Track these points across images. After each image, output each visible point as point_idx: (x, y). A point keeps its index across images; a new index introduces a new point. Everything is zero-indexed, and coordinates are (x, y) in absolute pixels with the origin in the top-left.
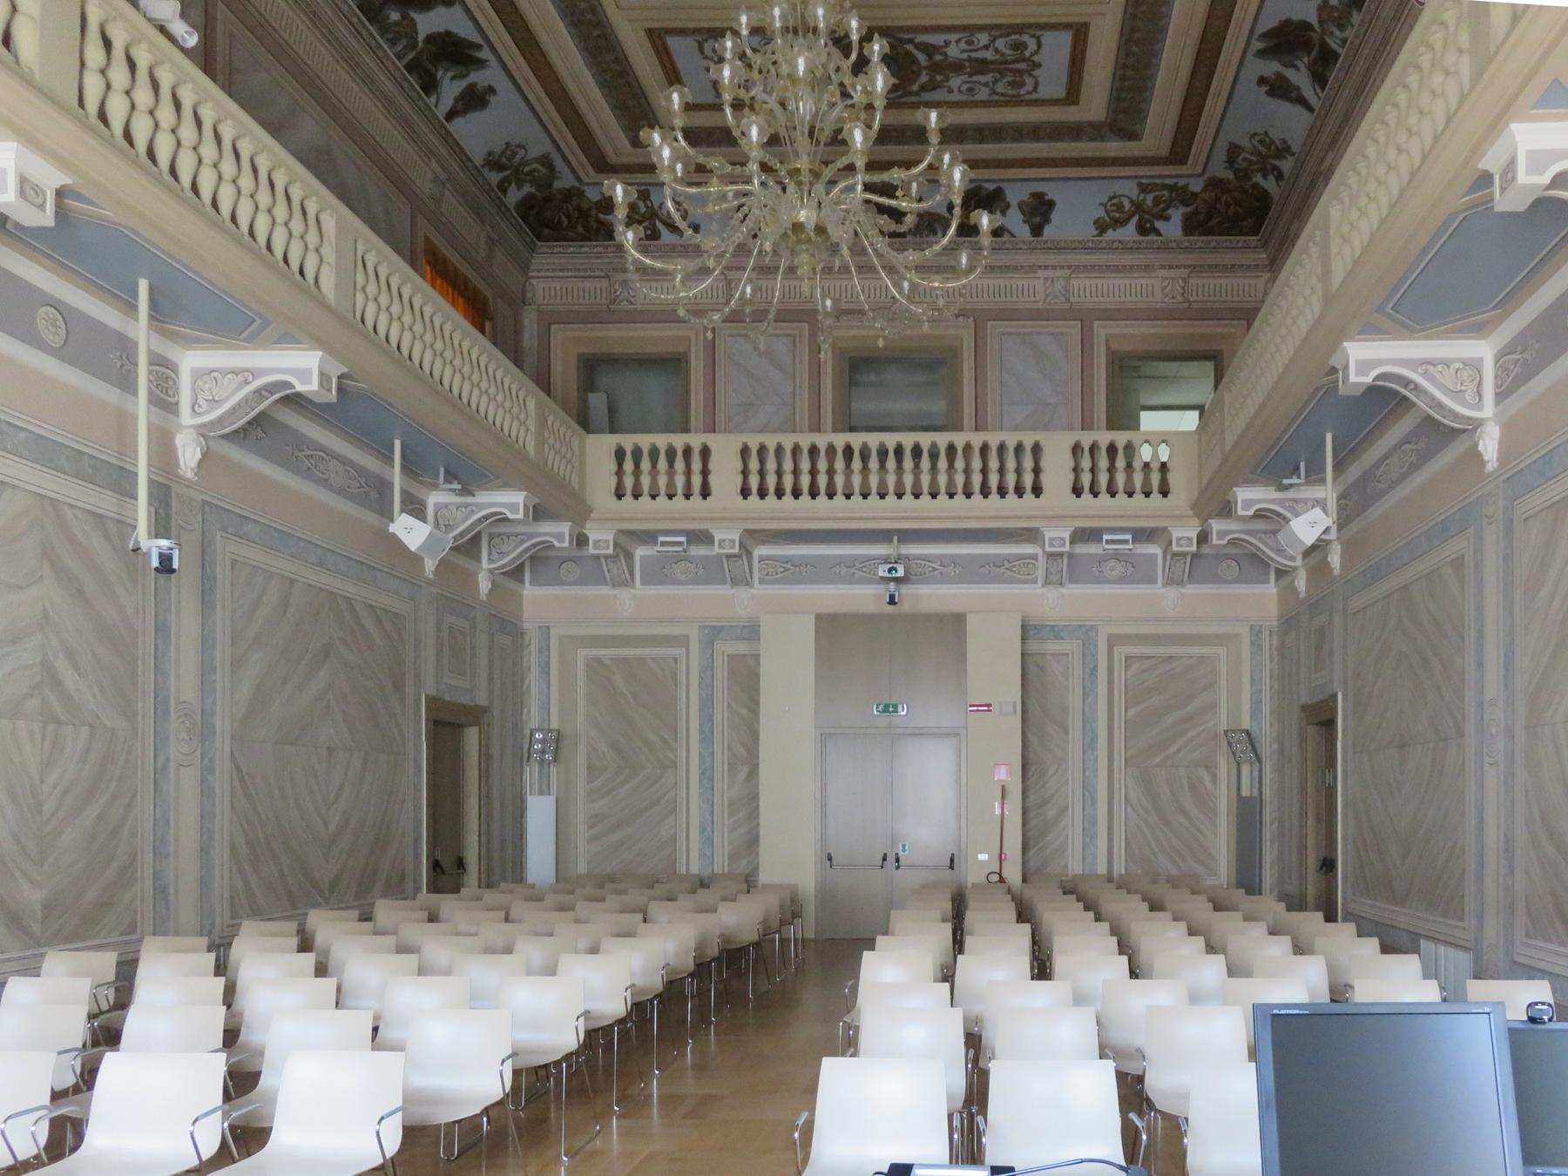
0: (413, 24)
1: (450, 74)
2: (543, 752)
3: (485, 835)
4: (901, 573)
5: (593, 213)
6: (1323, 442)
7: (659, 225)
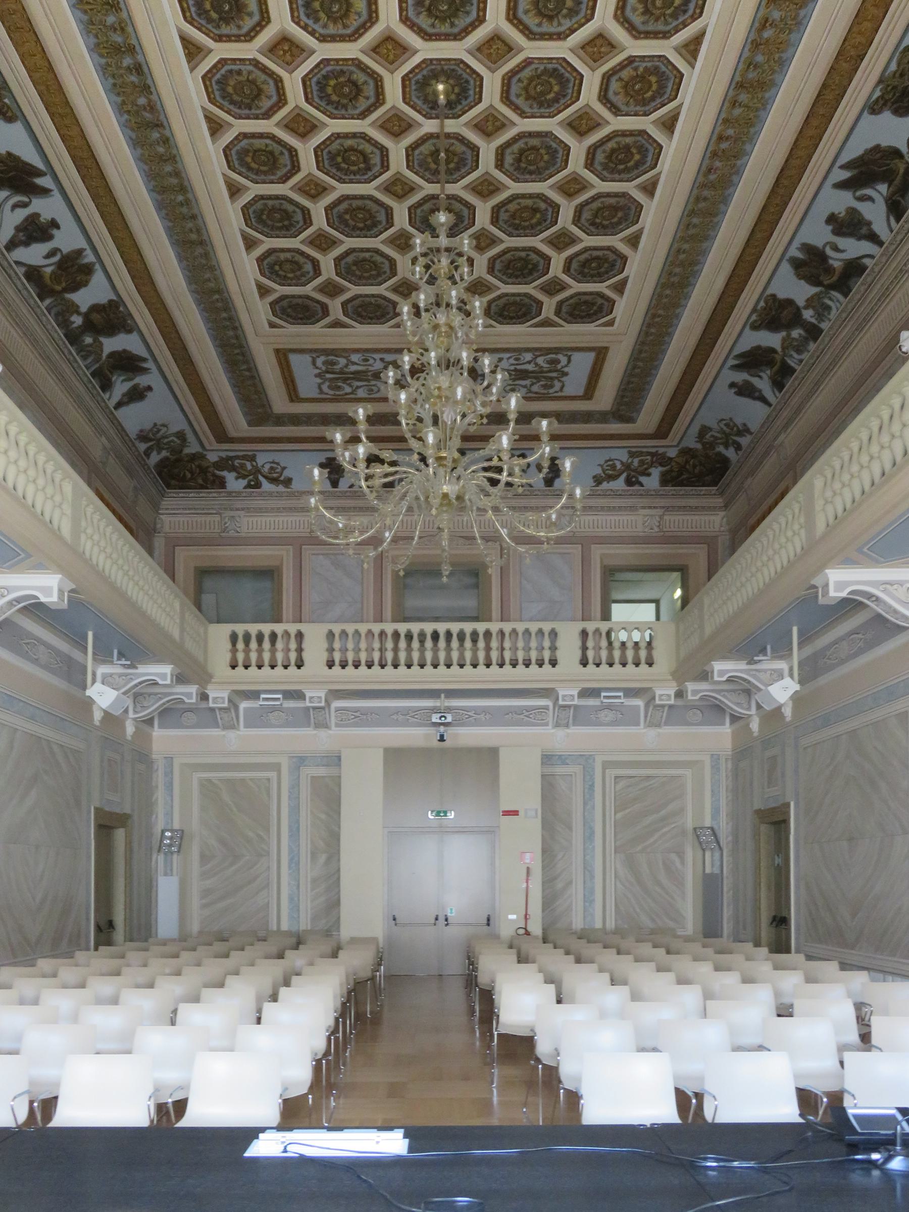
0: (101, 344)
1: (122, 378)
2: (170, 845)
3: (129, 906)
4: (449, 719)
5: (211, 469)
6: (791, 631)
7: (261, 478)
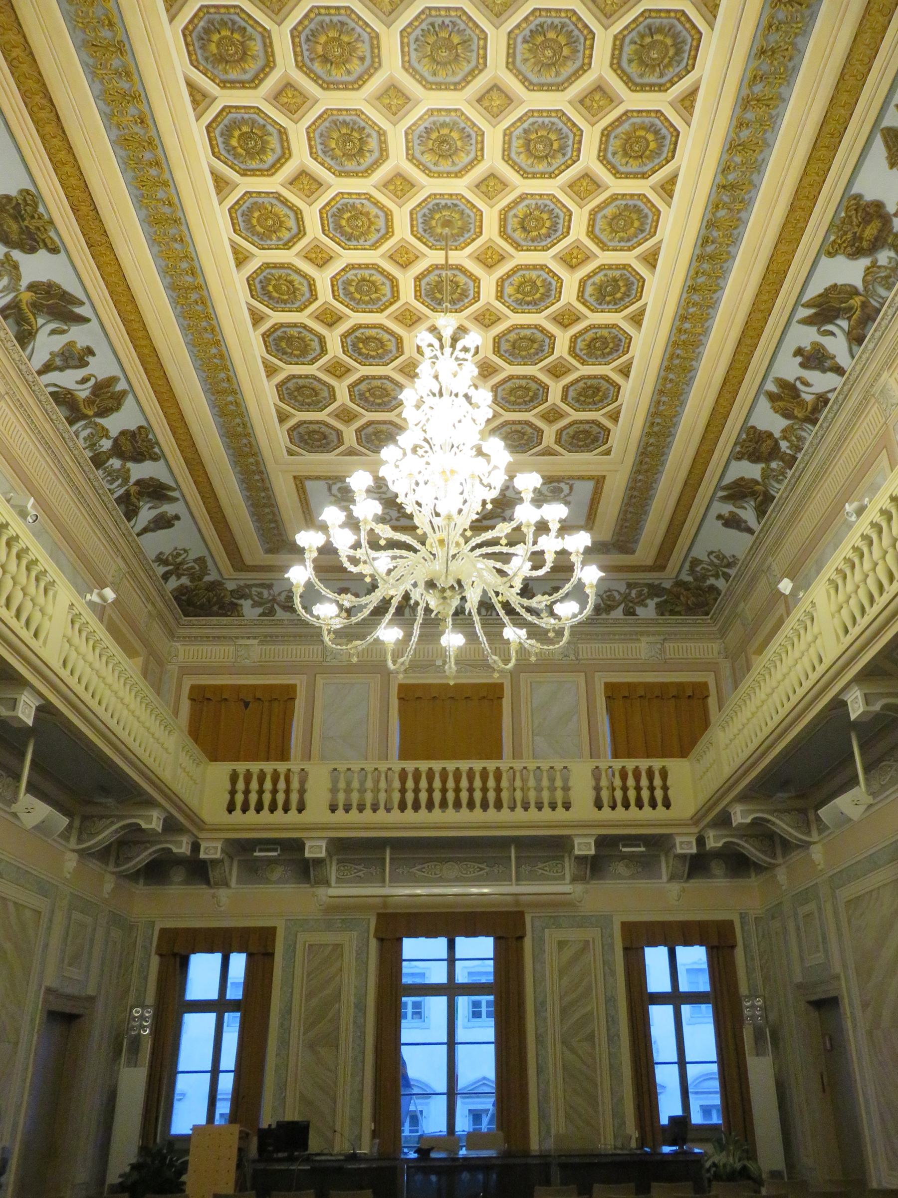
7: (276, 606)
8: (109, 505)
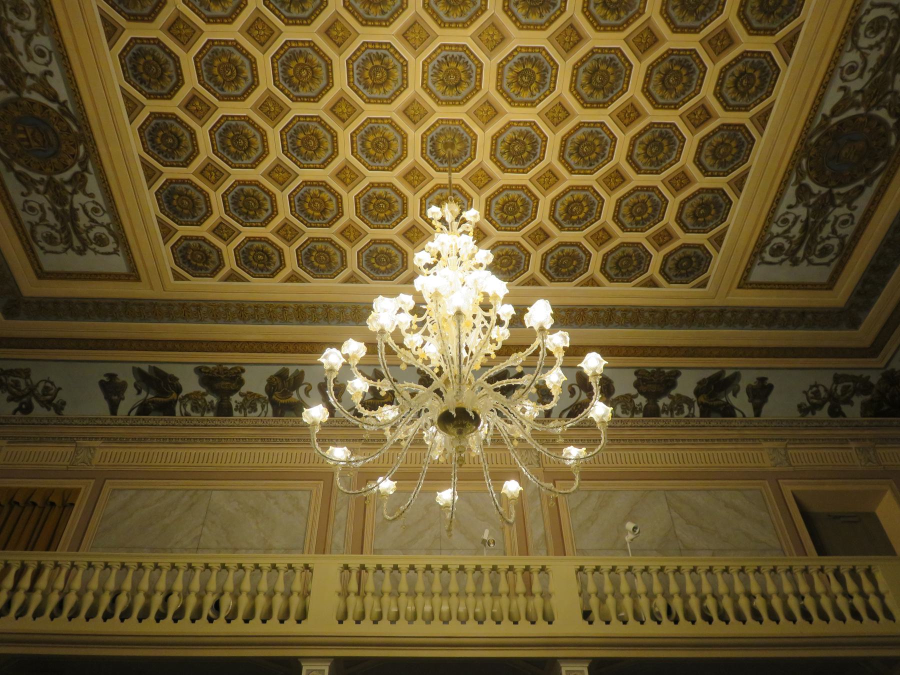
1: (730, 395)
8: (702, 424)
